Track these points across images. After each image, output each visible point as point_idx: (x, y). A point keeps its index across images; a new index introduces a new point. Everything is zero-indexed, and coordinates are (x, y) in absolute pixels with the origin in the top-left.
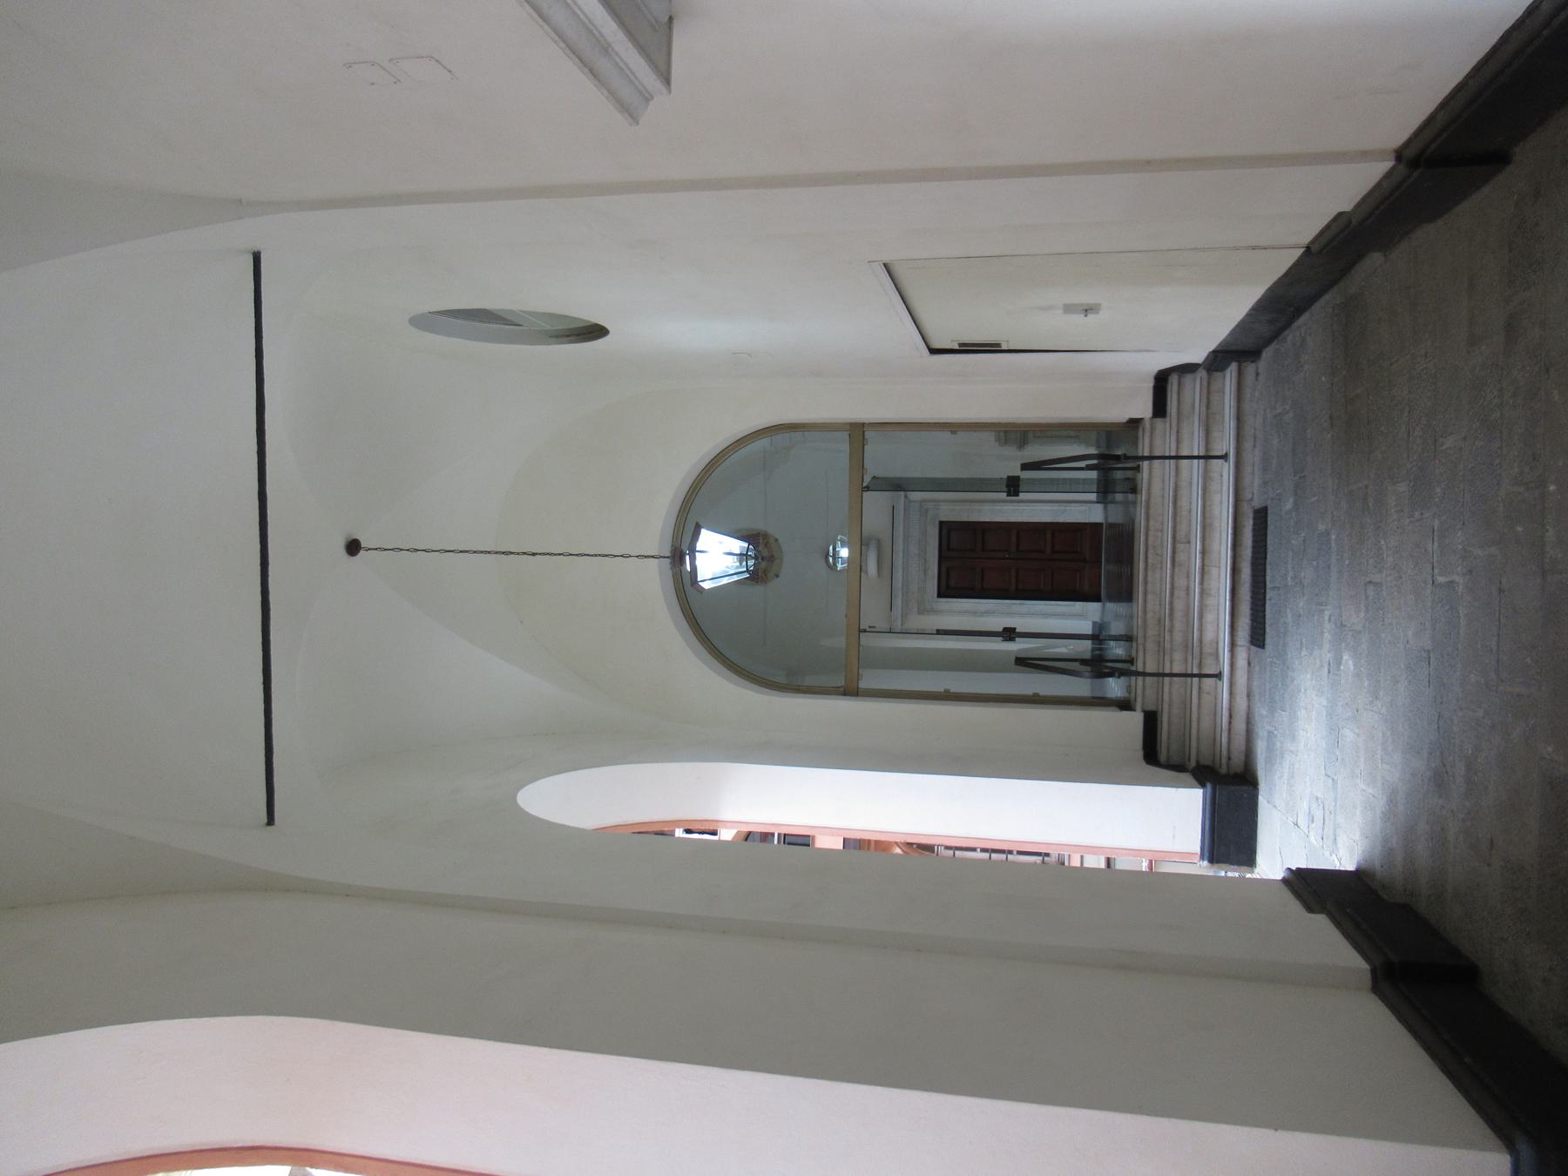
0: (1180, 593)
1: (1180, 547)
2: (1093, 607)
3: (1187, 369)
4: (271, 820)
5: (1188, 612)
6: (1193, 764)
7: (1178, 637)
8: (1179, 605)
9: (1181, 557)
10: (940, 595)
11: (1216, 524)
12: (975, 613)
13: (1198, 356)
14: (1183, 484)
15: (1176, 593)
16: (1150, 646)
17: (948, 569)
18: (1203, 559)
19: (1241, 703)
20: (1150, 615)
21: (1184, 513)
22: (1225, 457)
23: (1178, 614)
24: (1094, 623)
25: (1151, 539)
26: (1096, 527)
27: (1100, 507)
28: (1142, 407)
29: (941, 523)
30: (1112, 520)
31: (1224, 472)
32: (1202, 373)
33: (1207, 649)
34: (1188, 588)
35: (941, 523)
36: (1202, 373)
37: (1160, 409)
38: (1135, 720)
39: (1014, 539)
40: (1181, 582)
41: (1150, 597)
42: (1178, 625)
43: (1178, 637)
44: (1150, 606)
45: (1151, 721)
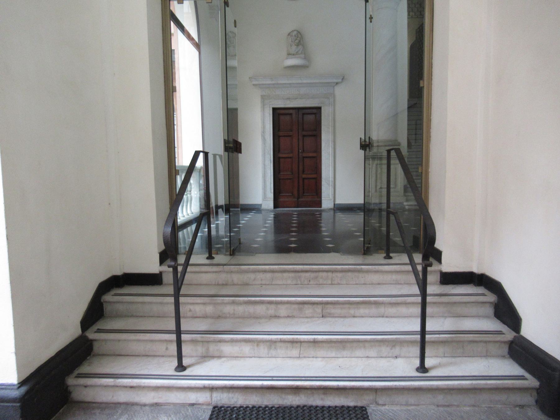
0: (272, 310)
1: (319, 309)
2: (270, 204)
3: (506, 311)
4: (235, 21)
5: (256, 317)
6: (91, 335)
7: (228, 309)
8: (260, 309)
9: (308, 310)
10: (274, 109)
11: (345, 353)
12: (263, 132)
13: (531, 331)
14: (382, 310)
15: (273, 306)
16: (223, 277)
17: (291, 114)
18: (309, 342)
19: (149, 398)
20: (252, 276)
21: (352, 312)
22: (422, 368)
23: (251, 309)
24: (261, 205)
25: (324, 274)
26: (319, 204)
27: (331, 206)
28: (451, 263)
29: (319, 109)
30: (324, 215)
31: (403, 366)
32: (509, 335)
33: (212, 348)
34: (277, 317)
35: (319, 109)
36: (509, 335)
37: (449, 279)
38: (152, 266)
39: (311, 155)
40: (283, 311)
41: (269, 275)
42: (240, 309)
43: (228, 309)
44: (260, 276)
45: (153, 280)
